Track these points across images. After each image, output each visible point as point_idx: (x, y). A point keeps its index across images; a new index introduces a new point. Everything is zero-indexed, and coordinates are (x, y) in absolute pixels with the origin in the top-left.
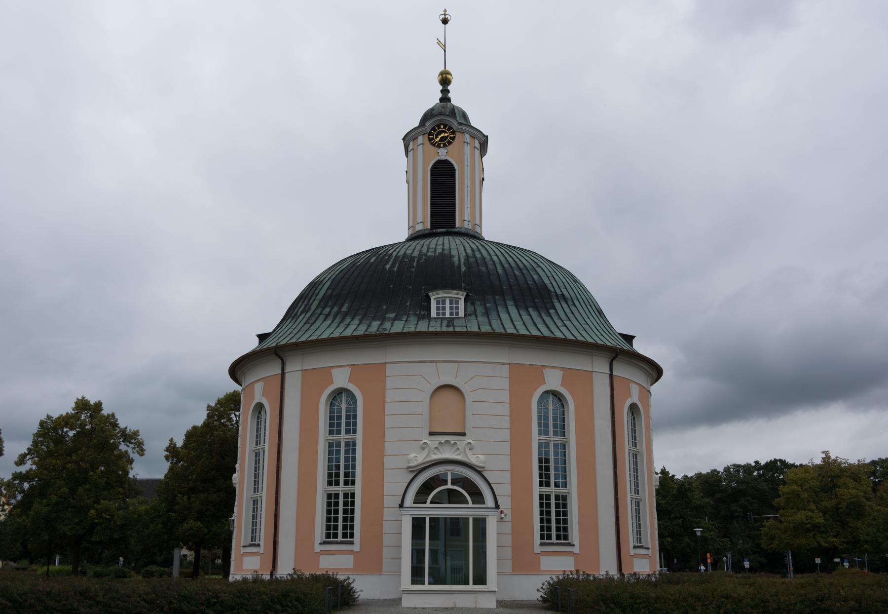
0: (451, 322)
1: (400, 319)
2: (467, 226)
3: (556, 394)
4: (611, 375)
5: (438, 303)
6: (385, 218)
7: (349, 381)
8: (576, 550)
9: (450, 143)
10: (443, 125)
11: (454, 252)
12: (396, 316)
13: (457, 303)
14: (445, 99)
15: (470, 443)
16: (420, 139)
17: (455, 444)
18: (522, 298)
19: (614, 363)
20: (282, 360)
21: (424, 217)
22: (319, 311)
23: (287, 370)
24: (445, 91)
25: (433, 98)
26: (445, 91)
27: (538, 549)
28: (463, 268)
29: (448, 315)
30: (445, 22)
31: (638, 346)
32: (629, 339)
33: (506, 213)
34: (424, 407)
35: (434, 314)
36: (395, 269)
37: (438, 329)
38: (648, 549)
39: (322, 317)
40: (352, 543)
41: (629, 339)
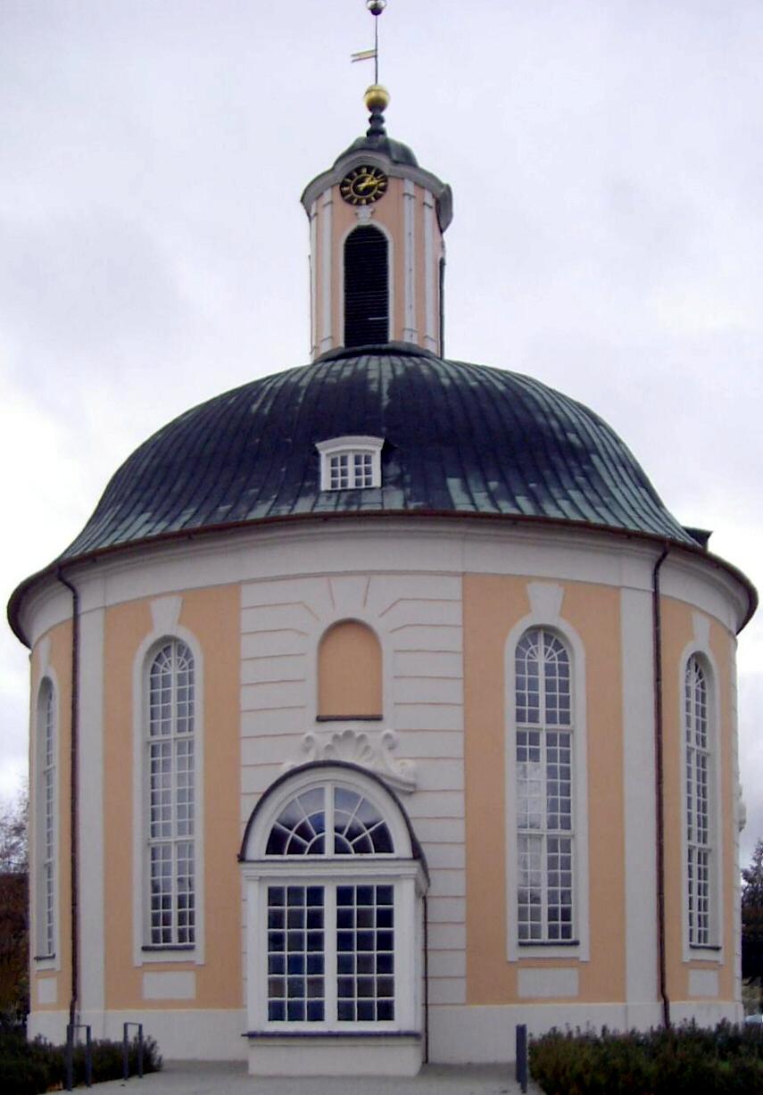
0: (357, 493)
1: (267, 499)
2: (409, 339)
3: (549, 634)
4: (656, 595)
5: (334, 463)
6: (273, 328)
7: (180, 622)
8: (582, 953)
9: (377, 197)
10: (371, 168)
11: (372, 375)
12: (260, 492)
13: (368, 460)
14: (376, 130)
15: (388, 737)
16: (328, 196)
17: (362, 738)
18: (507, 457)
19: (662, 570)
20: (73, 590)
21: (334, 328)
22: (135, 497)
23: (84, 606)
24: (376, 120)
25: (361, 128)
26: (376, 120)
27: (514, 953)
28: (386, 401)
29: (351, 485)
30: (376, 11)
31: (713, 547)
32: (702, 536)
33: (487, 318)
34: (307, 666)
35: (325, 484)
36: (266, 411)
37: (331, 509)
38: (717, 949)
39: (140, 507)
40: (191, 948)
41: (702, 536)
